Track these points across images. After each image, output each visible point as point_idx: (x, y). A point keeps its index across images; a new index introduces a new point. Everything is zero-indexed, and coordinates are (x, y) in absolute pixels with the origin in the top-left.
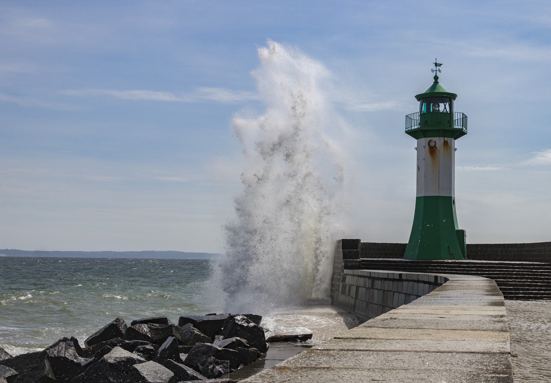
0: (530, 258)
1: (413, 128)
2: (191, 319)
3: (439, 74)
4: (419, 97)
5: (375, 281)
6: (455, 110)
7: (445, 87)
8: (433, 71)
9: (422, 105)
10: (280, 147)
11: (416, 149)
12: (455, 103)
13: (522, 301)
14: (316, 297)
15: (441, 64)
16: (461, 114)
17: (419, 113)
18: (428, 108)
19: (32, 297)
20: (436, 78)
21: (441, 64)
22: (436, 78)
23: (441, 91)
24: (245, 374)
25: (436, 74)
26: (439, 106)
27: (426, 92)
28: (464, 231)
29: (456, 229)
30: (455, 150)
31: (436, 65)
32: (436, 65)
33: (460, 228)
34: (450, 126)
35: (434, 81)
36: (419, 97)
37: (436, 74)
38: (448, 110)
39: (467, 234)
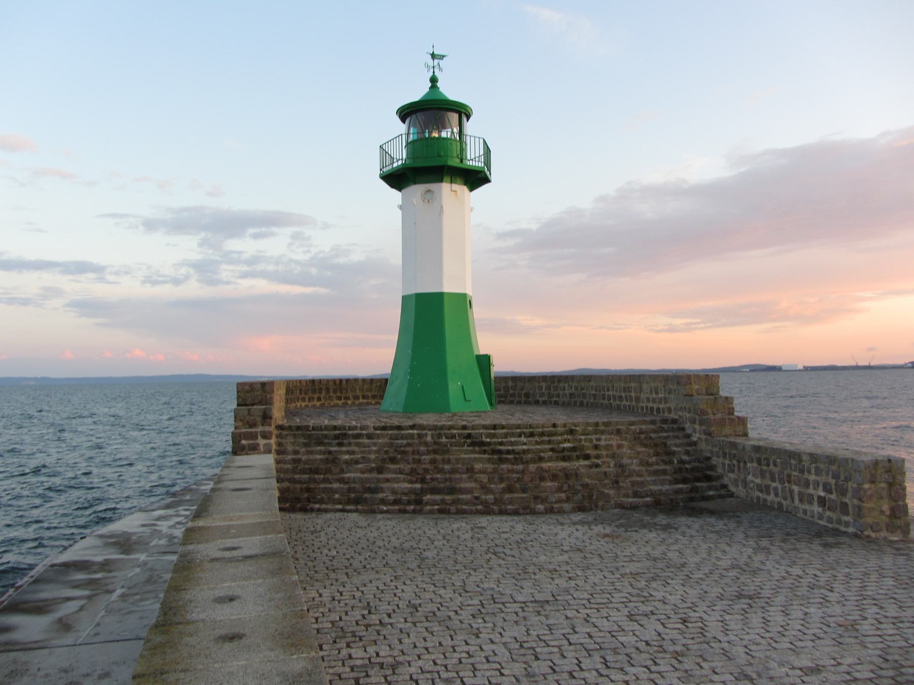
0: (603, 401)
1: (395, 165)
3: (437, 74)
4: (405, 113)
7: (450, 91)
11: (401, 207)
15: (444, 56)
16: (482, 141)
17: (404, 136)
19: (652, 499)
20: (434, 80)
21: (444, 56)
22: (434, 80)
23: (441, 98)
24: (244, 442)
25: (434, 72)
27: (425, 99)
28: (489, 356)
29: (476, 353)
30: (472, 209)
31: (433, 56)
32: (433, 56)
33: (482, 351)
34: (462, 161)
35: (430, 85)
36: (405, 113)
37: (434, 72)
39: (494, 360)
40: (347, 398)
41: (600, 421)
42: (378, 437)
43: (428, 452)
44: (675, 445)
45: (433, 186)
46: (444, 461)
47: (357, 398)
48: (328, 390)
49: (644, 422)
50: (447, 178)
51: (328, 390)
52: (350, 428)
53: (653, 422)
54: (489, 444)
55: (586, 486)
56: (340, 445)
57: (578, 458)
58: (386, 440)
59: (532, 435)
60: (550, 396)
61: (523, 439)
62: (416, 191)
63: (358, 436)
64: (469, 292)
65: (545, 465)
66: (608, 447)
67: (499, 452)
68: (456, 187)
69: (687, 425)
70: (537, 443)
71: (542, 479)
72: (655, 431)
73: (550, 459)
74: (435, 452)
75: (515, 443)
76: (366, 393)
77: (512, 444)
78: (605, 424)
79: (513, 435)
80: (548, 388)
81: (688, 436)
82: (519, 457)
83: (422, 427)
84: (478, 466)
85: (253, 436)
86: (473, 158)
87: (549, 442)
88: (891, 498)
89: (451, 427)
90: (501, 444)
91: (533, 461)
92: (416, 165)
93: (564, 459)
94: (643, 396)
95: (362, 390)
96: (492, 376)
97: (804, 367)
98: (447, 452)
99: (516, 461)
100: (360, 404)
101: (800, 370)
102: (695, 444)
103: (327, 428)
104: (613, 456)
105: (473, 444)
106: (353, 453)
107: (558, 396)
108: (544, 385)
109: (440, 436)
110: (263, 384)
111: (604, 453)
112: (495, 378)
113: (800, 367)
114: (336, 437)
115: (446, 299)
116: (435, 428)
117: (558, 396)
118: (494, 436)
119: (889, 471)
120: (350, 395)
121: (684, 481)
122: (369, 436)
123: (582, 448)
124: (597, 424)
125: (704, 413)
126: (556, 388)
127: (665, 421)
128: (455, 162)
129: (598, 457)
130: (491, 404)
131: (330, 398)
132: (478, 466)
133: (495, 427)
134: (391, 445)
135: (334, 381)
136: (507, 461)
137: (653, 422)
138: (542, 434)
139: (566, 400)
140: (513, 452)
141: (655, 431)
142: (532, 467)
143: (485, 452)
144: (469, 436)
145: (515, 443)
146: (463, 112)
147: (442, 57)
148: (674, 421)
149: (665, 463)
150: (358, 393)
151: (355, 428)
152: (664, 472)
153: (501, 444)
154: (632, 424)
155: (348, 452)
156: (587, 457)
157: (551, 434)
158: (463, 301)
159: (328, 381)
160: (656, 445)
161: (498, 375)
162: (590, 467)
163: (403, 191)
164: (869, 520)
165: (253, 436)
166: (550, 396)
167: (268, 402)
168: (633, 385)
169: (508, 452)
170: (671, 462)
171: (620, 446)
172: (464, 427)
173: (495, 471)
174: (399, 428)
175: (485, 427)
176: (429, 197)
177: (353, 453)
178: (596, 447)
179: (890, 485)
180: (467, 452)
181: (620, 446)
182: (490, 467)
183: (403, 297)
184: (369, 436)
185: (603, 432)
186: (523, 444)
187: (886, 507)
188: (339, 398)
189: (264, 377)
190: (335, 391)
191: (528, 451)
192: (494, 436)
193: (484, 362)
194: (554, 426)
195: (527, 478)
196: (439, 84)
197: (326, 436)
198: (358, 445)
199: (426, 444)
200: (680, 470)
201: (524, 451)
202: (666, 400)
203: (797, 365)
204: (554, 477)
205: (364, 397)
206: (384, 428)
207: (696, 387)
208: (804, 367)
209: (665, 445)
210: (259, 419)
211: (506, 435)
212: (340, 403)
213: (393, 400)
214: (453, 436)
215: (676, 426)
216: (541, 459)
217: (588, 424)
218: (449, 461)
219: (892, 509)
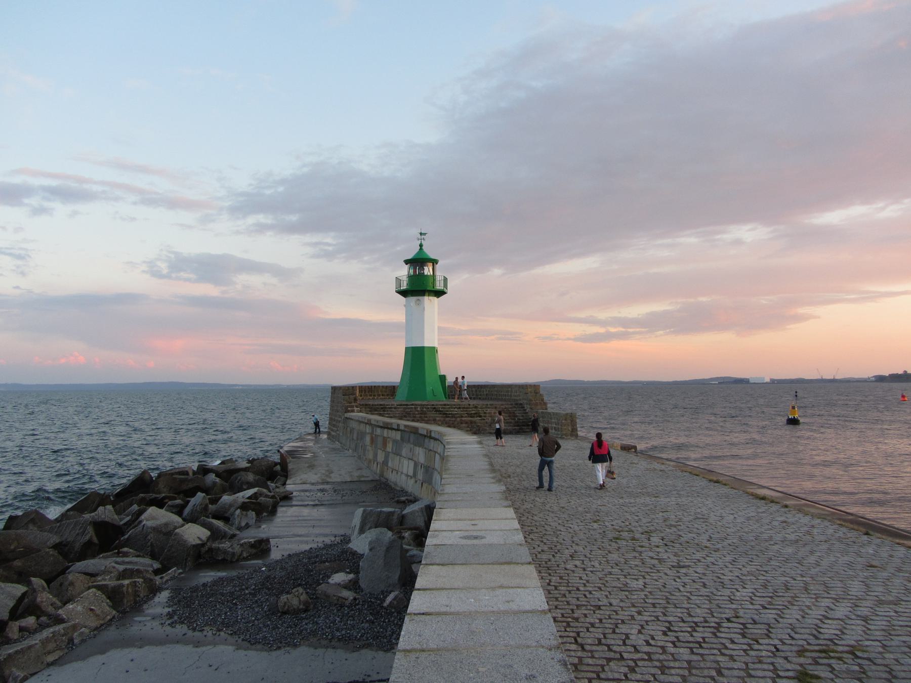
1: (402, 288)
2: (212, 469)
4: (407, 262)
5: (549, 413)
6: (438, 273)
7: (430, 253)
8: (419, 239)
9: (282, 506)
10: (362, 591)
11: (405, 306)
12: (437, 267)
13: (794, 489)
14: (15, 601)
18: (415, 271)
20: (421, 246)
22: (421, 246)
23: (425, 257)
26: (424, 269)
31: (421, 234)
32: (421, 234)
35: (419, 248)
38: (432, 274)
40: (374, 396)
41: (489, 403)
42: (399, 408)
43: (419, 414)
44: (518, 413)
45: (420, 298)
46: (425, 417)
47: (379, 395)
48: (365, 391)
49: (508, 404)
50: (427, 294)
51: (365, 391)
52: (387, 405)
53: (511, 404)
54: (443, 411)
55: (478, 426)
56: (384, 411)
57: (477, 417)
58: (402, 409)
59: (460, 408)
60: (477, 395)
61: (456, 410)
62: (413, 300)
63: (391, 408)
64: (436, 345)
65: (463, 419)
66: (489, 413)
67: (446, 414)
68: (431, 298)
69: (525, 406)
70: (462, 411)
71: (462, 423)
72: (511, 408)
73: (466, 417)
74: (421, 414)
75: (453, 411)
76: (384, 393)
77: (451, 411)
78: (490, 405)
79: (452, 408)
80: (476, 391)
81: (525, 410)
82: (453, 416)
83: (416, 405)
84: (438, 419)
85: (352, 407)
86: (439, 286)
87: (466, 411)
88: (572, 426)
89: (428, 405)
90: (447, 411)
91: (459, 417)
92: (413, 289)
93: (471, 417)
94: (513, 394)
95: (382, 391)
96: (447, 385)
97: (771, 380)
98: (426, 414)
99: (452, 417)
100: (381, 399)
101: (766, 383)
102: (527, 413)
103: (377, 405)
104: (491, 417)
105: (436, 411)
106: (389, 414)
107: (481, 395)
108: (474, 389)
109: (423, 408)
110: (353, 387)
111: (488, 415)
112: (468, 386)
113: (767, 380)
114: (382, 408)
115: (426, 350)
116: (421, 405)
117: (481, 395)
118: (444, 408)
119: (571, 416)
120: (376, 394)
121: (518, 426)
122: (395, 408)
123: (479, 413)
124: (487, 405)
125: (531, 400)
126: (480, 391)
127: (517, 404)
128: (430, 288)
129: (485, 417)
130: (446, 398)
131: (366, 395)
132: (438, 419)
133: (445, 405)
134: (404, 411)
135: (368, 387)
136: (449, 417)
137: (511, 404)
138: (464, 408)
139: (484, 397)
140: (451, 414)
141: (511, 408)
142: (458, 419)
143: (440, 414)
144: (435, 408)
145: (453, 411)
146: (434, 262)
147: (425, 234)
148: (521, 404)
149: (512, 419)
150: (380, 393)
151: (389, 405)
152: (511, 423)
153: (447, 411)
154: (502, 405)
155: (387, 414)
156: (480, 416)
157: (467, 408)
158: (433, 350)
159: (365, 386)
160: (510, 413)
161: (469, 384)
162: (481, 420)
163: (408, 298)
164: (564, 433)
165: (352, 407)
166: (477, 395)
167: (355, 394)
168: (510, 389)
169: (450, 414)
170: (514, 419)
171: (495, 413)
172: (433, 405)
173: (444, 420)
174: (407, 405)
175: (441, 405)
176: (418, 303)
177: (389, 414)
178: (485, 413)
179: (572, 421)
180: (433, 414)
181: (495, 413)
182: (442, 419)
183: (406, 348)
184: (395, 408)
185: (489, 408)
186: (456, 411)
187: (570, 429)
188: (371, 395)
189: (239, 385)
190: (368, 392)
191: (457, 414)
192: (444, 408)
193: (443, 378)
194: (469, 405)
195: (456, 423)
196: (423, 248)
197: (378, 408)
198: (391, 411)
199: (417, 411)
200: (518, 422)
201: (456, 414)
202: (519, 395)
203: (764, 378)
204: (466, 423)
205: (383, 395)
206: (401, 405)
207: (530, 390)
208: (771, 380)
209: (514, 413)
210: (353, 401)
211: (449, 408)
212: (371, 398)
213: (401, 397)
214: (429, 408)
215: (521, 406)
216: (462, 417)
217: (483, 405)
218: (426, 417)
219: (572, 429)
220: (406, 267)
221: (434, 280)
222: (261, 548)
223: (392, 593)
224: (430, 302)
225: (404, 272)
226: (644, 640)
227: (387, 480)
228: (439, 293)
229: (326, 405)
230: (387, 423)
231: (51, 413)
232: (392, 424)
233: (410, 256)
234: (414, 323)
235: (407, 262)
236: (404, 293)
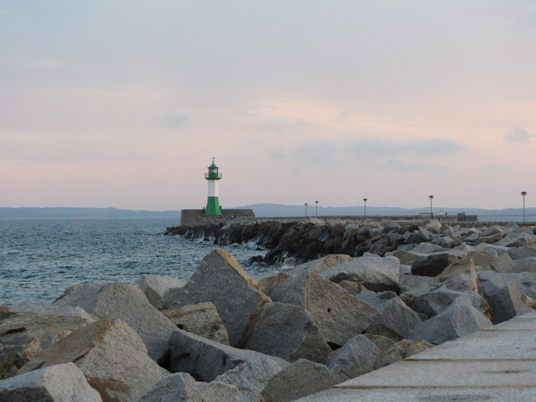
4: (208, 168)
12: (218, 169)
20: (213, 162)
22: (213, 162)
32: (213, 158)
62: (211, 181)
86: (219, 177)
146: (218, 168)
147: (214, 158)
158: (217, 197)
176: (213, 182)
193: (221, 207)
220: (208, 169)
221: (218, 174)
222: (189, 293)
223: (302, 359)
224: (217, 182)
225: (207, 171)
226: (328, 343)
227: (379, 281)
228: (219, 179)
229: (180, 214)
230: (411, 220)
231: (117, 238)
232: (415, 220)
233: (209, 167)
234: (211, 189)
235: (208, 168)
236: (207, 179)
